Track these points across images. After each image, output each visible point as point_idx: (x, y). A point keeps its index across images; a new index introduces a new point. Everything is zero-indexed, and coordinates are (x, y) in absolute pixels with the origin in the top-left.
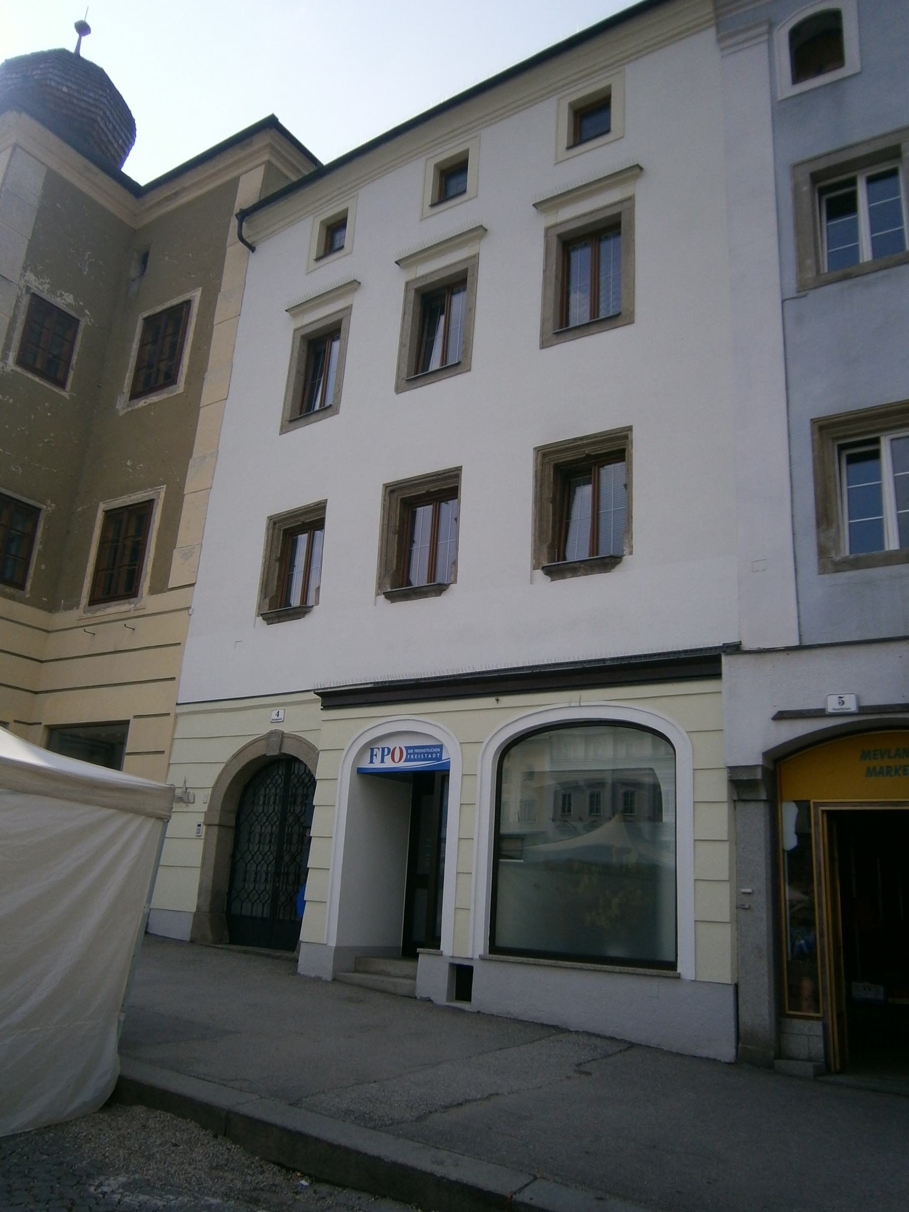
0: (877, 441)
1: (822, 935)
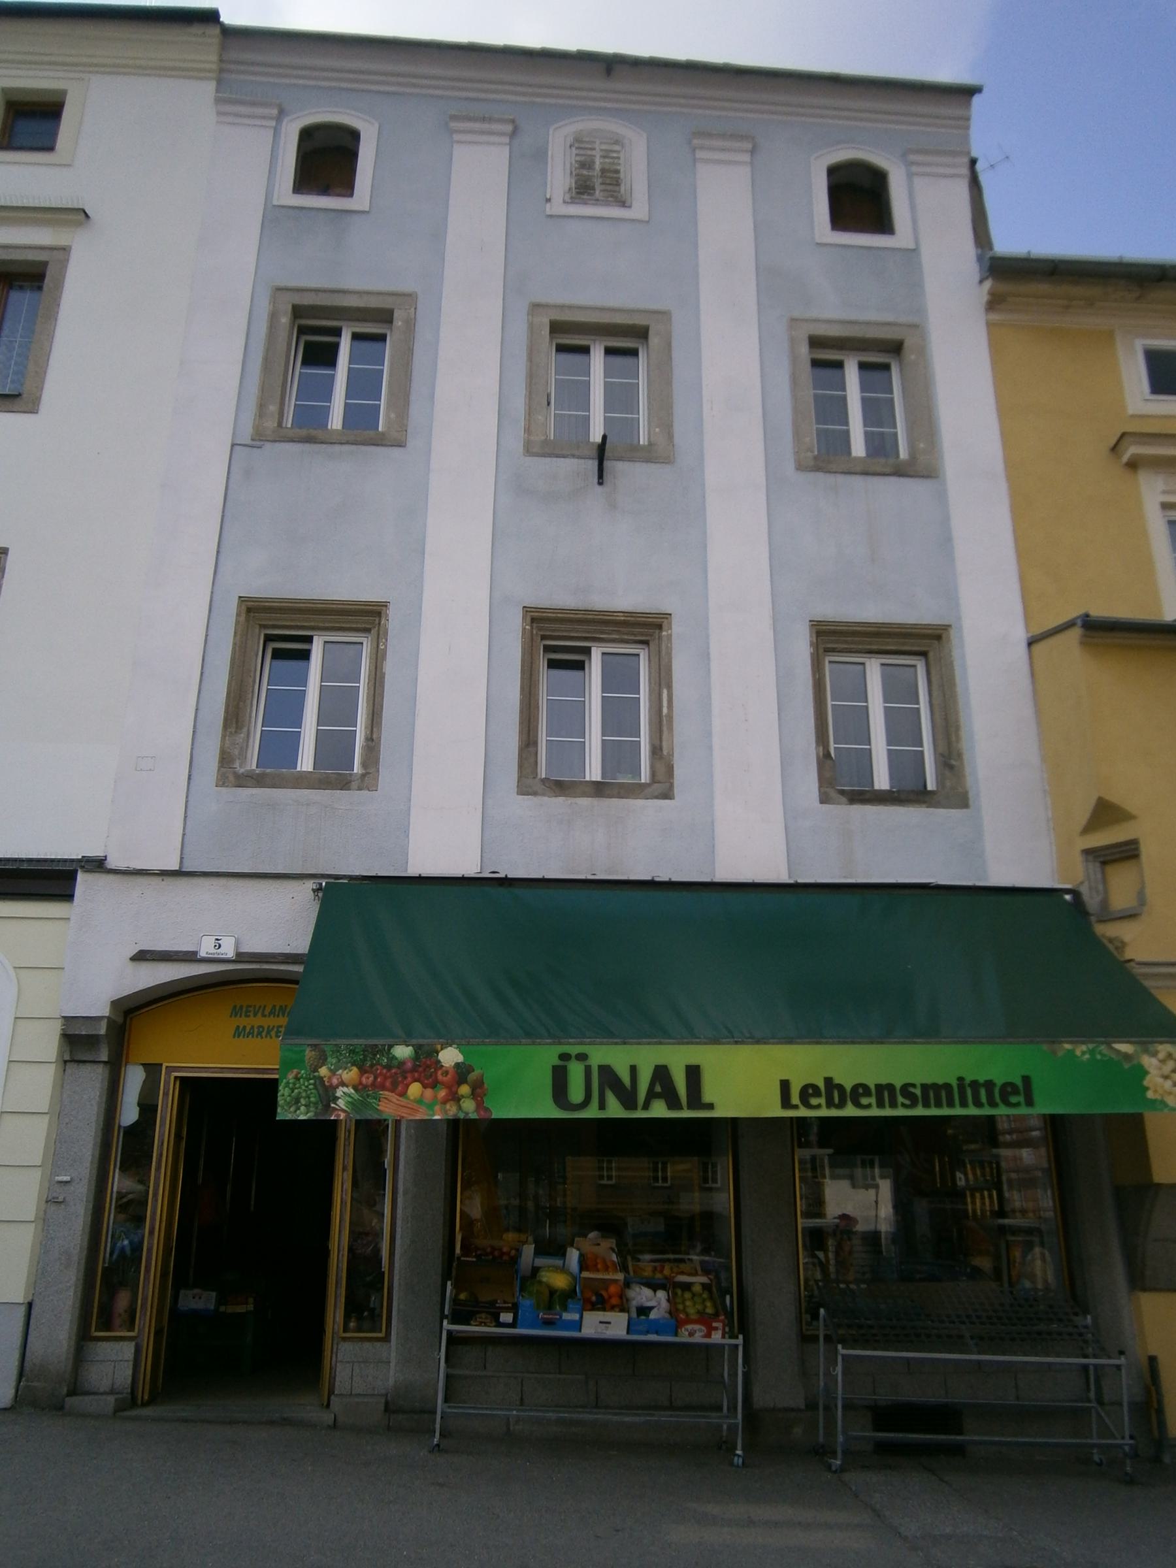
0: (309, 640)
1: (151, 1232)
